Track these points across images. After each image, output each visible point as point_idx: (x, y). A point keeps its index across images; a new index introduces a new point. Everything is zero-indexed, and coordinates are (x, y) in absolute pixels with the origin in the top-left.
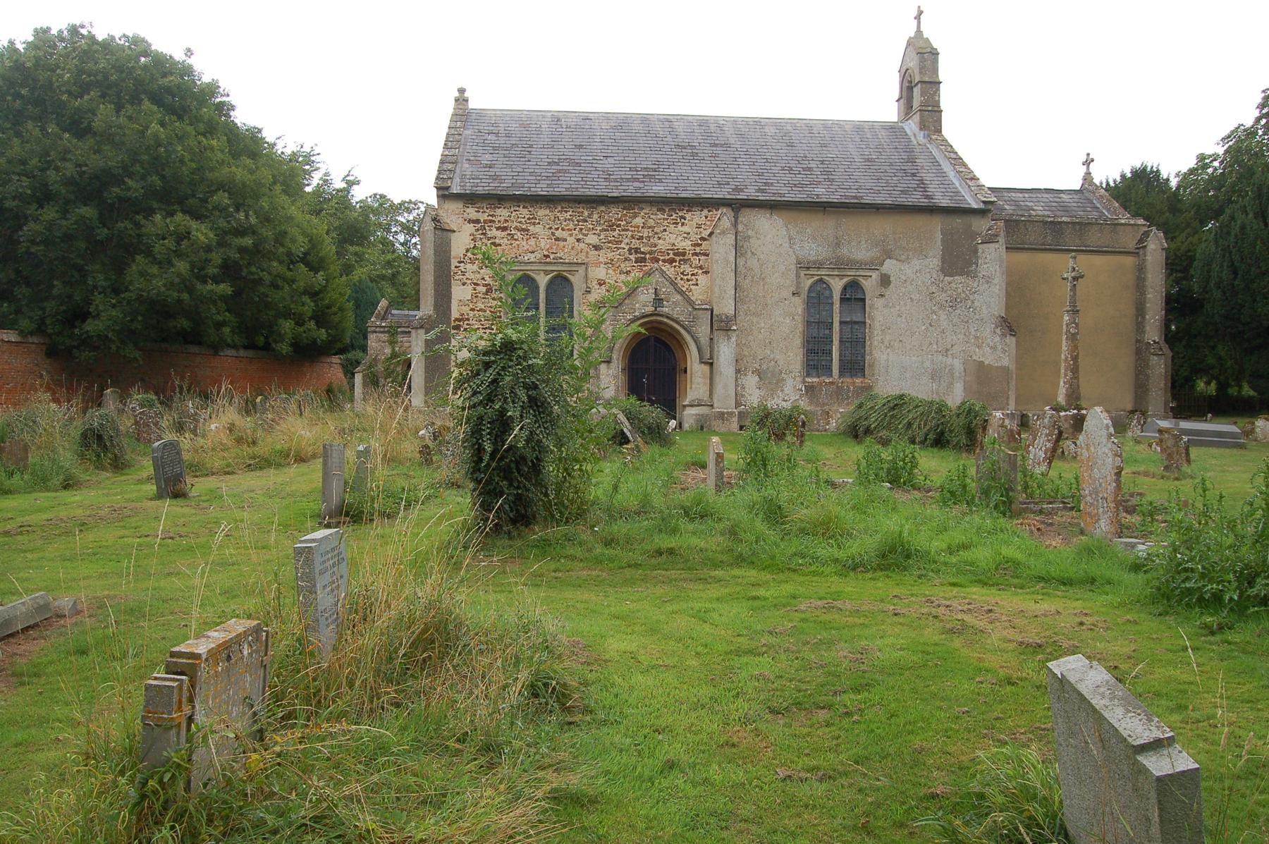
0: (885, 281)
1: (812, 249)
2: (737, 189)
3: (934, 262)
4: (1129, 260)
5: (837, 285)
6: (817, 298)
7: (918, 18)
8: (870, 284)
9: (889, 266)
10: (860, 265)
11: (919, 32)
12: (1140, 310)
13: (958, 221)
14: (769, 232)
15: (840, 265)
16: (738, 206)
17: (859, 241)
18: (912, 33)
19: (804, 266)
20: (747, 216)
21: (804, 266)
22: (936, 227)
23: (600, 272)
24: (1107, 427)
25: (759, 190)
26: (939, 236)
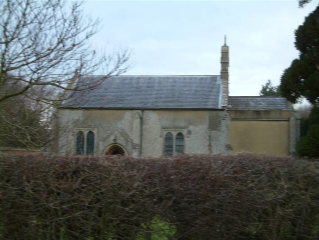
0: (189, 132)
1: (166, 123)
2: (145, 104)
3: (206, 126)
4: (286, 123)
5: (175, 134)
6: (168, 138)
7: (225, 39)
8: (185, 133)
9: (191, 128)
10: (181, 128)
11: (225, 44)
12: (289, 141)
13: (214, 113)
14: (152, 118)
15: (175, 128)
16: (143, 110)
17: (182, 119)
18: (223, 45)
19: (164, 128)
20: (146, 112)
21: (164, 128)
22: (206, 114)
23: (218, 226)
24: (140, 148)
25: (152, 105)
26: (207, 118)
